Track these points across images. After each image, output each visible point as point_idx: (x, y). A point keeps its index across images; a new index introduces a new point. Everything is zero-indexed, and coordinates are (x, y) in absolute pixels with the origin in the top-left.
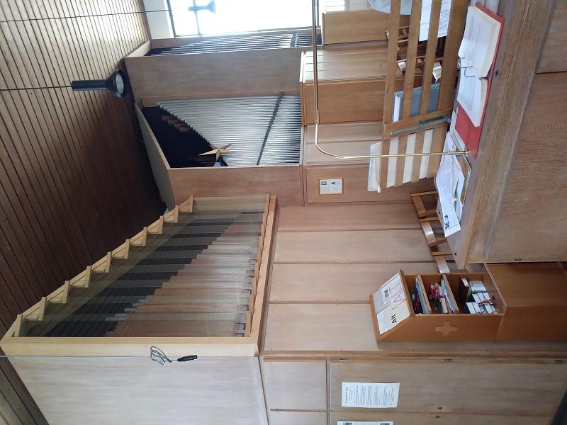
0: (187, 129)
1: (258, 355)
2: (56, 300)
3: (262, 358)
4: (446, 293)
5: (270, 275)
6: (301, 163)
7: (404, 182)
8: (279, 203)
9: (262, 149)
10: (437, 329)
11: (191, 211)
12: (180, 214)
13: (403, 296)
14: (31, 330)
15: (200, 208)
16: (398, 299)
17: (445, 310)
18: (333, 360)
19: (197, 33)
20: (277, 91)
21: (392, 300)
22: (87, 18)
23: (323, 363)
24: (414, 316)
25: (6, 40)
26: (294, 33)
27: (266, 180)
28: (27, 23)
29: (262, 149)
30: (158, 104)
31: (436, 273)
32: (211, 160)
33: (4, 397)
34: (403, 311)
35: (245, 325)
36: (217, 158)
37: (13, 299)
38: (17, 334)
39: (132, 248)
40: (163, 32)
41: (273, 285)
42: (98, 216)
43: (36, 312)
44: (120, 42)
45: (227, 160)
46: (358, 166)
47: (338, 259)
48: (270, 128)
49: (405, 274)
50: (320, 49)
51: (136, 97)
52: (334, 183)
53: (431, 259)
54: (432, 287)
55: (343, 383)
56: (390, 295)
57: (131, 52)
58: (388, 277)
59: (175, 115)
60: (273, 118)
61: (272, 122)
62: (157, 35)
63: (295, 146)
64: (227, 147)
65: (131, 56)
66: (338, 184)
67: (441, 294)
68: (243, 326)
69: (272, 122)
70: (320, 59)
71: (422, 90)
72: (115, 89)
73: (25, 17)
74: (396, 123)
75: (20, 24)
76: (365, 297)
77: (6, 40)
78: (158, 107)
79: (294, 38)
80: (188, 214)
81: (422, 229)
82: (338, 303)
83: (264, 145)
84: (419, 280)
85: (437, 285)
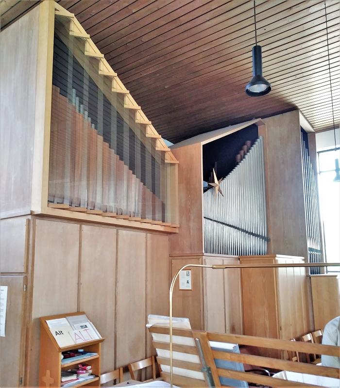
0: (238, 161)
1: (32, 214)
2: (87, 45)
3: (30, 217)
4: (81, 380)
5: (107, 226)
6: (205, 254)
7: (157, 349)
8: (173, 235)
9: (219, 222)
10: (48, 372)
11: (166, 161)
12: (163, 153)
13: (80, 341)
14: (60, 25)
15: (169, 169)
16: (77, 337)
17: (64, 379)
18: (26, 278)
19: (321, 171)
20: (271, 236)
21: (77, 332)
22: (332, 85)
23: (22, 270)
25: (310, 7)
26: (321, 251)
27: (192, 224)
28: (324, 26)
29: (219, 222)
30: (261, 137)
31: (100, 371)
32: (208, 177)
33: (12, 7)
34: (64, 342)
35: (62, 203)
37: (93, 14)
38: (57, 13)
39: (133, 112)
40: (321, 142)
41: (97, 229)
42: (166, 87)
43: (77, 29)
45: (209, 192)
46: (202, 303)
47: (120, 285)
48: (238, 229)
49: (100, 344)
50: (307, 271)
51: (266, 120)
52: (188, 282)
53: (117, 366)
54: (89, 367)
55: (7, 287)
56: (82, 330)
58: (98, 327)
60: (247, 232)
62: (318, 136)
63: (223, 250)
65: (301, 116)
67: (81, 375)
68: (93, 208)
70: (125, 204)
71: (240, 372)
73: (329, 24)
74: (207, 344)
76: (83, 308)
77: (310, 7)
78: (257, 137)
79: (317, 251)
80: (163, 160)
81: (146, 358)
82: (79, 284)
83: (223, 223)
84: (94, 355)
85: (91, 371)
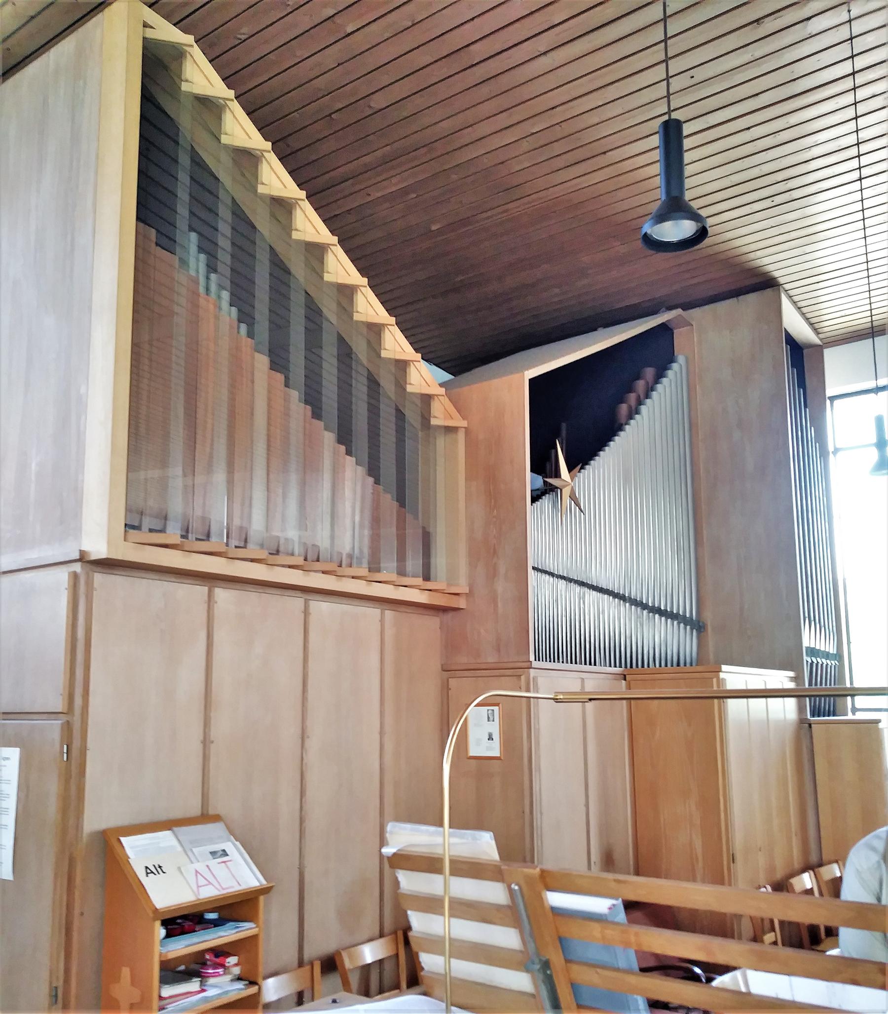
1: (83, 558)
3: (77, 567)
4: (211, 992)
6: (535, 664)
7: (409, 912)
10: (126, 972)
11: (434, 422)
12: (427, 399)
13: (209, 892)
15: (441, 442)
16: (202, 881)
17: (167, 991)
18: (68, 728)
19: (838, 446)
20: (709, 617)
21: (200, 867)
23: (57, 703)
24: (155, 919)
25: (809, 19)
26: (839, 656)
28: (846, 68)
30: (681, 359)
31: (262, 970)
33: (32, 18)
35: (162, 531)
36: (549, 480)
37: (243, 37)
38: (150, 34)
41: (253, 597)
44: (815, 277)
45: (546, 502)
47: (314, 744)
48: (622, 597)
49: (262, 898)
50: (801, 709)
52: (490, 738)
54: (232, 960)
56: (214, 863)
57: (794, 303)
59: (654, 394)
60: (644, 606)
61: (635, 603)
64: (578, 504)
65: (785, 302)
66: (488, 749)
67: (211, 981)
68: (242, 544)
69: (635, 603)
72: (661, 217)
73: (861, 62)
74: (541, 900)
75: (844, 51)
77: (809, 19)
78: (672, 359)
79: (827, 655)
80: (426, 418)
81: (381, 935)
82: (206, 742)
83: (582, 584)
84: (246, 929)
85: (237, 971)
